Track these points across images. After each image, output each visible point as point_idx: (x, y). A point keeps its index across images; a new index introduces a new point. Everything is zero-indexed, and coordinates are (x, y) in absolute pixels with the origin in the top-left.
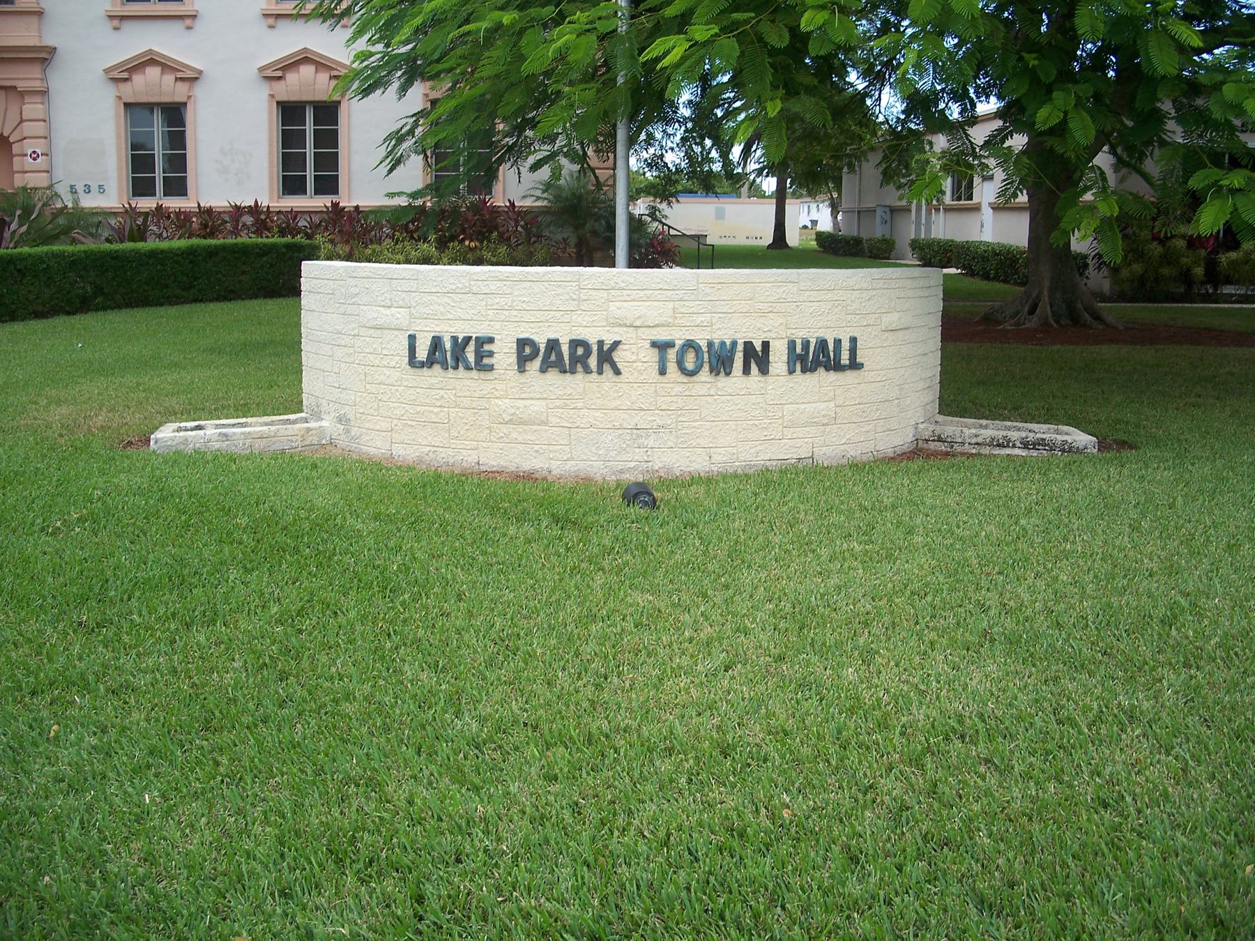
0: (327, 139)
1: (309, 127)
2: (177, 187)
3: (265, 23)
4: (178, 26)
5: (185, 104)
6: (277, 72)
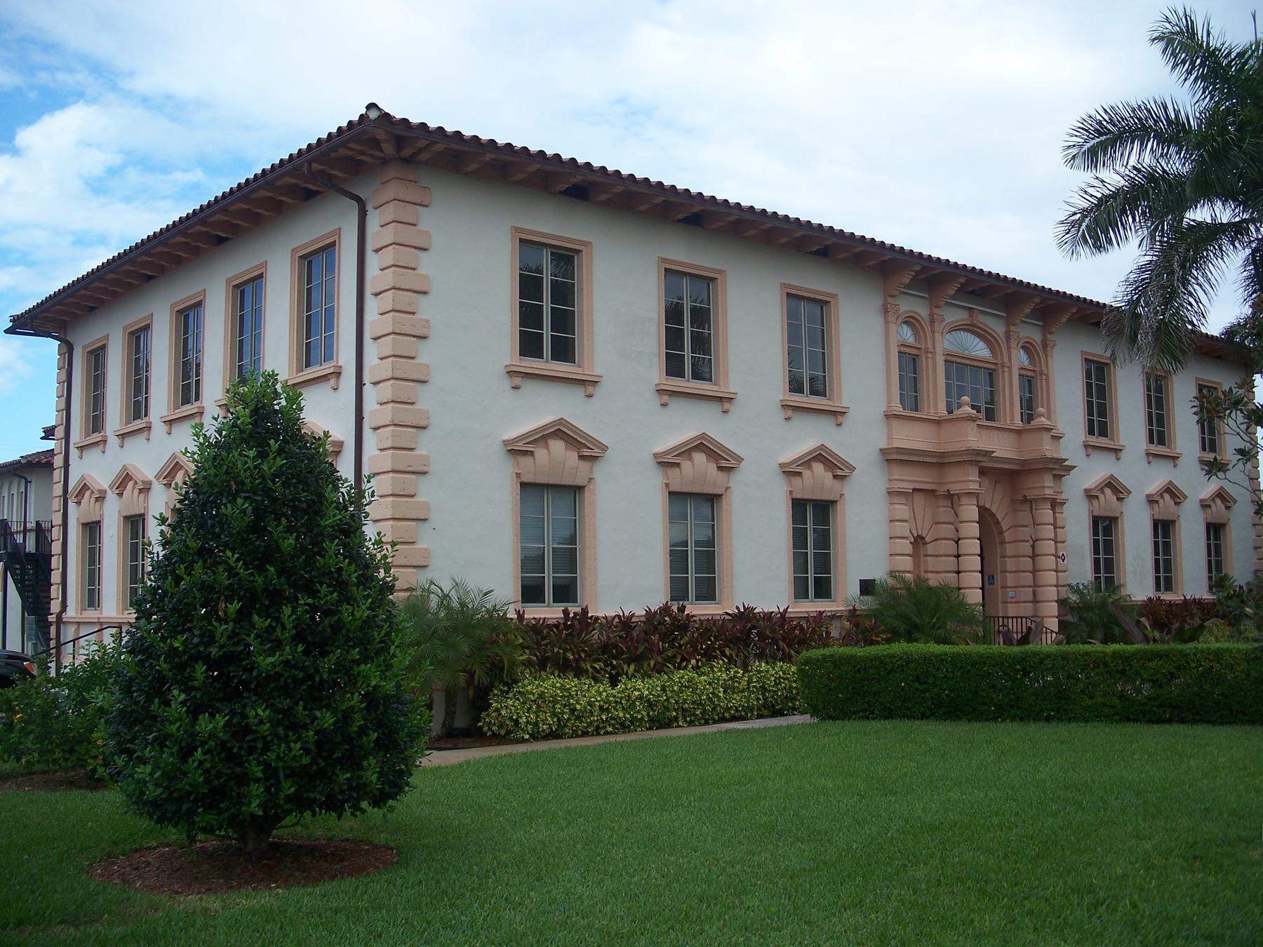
2: (708, 592)
3: (506, 384)
5: (834, 502)
6: (517, 450)
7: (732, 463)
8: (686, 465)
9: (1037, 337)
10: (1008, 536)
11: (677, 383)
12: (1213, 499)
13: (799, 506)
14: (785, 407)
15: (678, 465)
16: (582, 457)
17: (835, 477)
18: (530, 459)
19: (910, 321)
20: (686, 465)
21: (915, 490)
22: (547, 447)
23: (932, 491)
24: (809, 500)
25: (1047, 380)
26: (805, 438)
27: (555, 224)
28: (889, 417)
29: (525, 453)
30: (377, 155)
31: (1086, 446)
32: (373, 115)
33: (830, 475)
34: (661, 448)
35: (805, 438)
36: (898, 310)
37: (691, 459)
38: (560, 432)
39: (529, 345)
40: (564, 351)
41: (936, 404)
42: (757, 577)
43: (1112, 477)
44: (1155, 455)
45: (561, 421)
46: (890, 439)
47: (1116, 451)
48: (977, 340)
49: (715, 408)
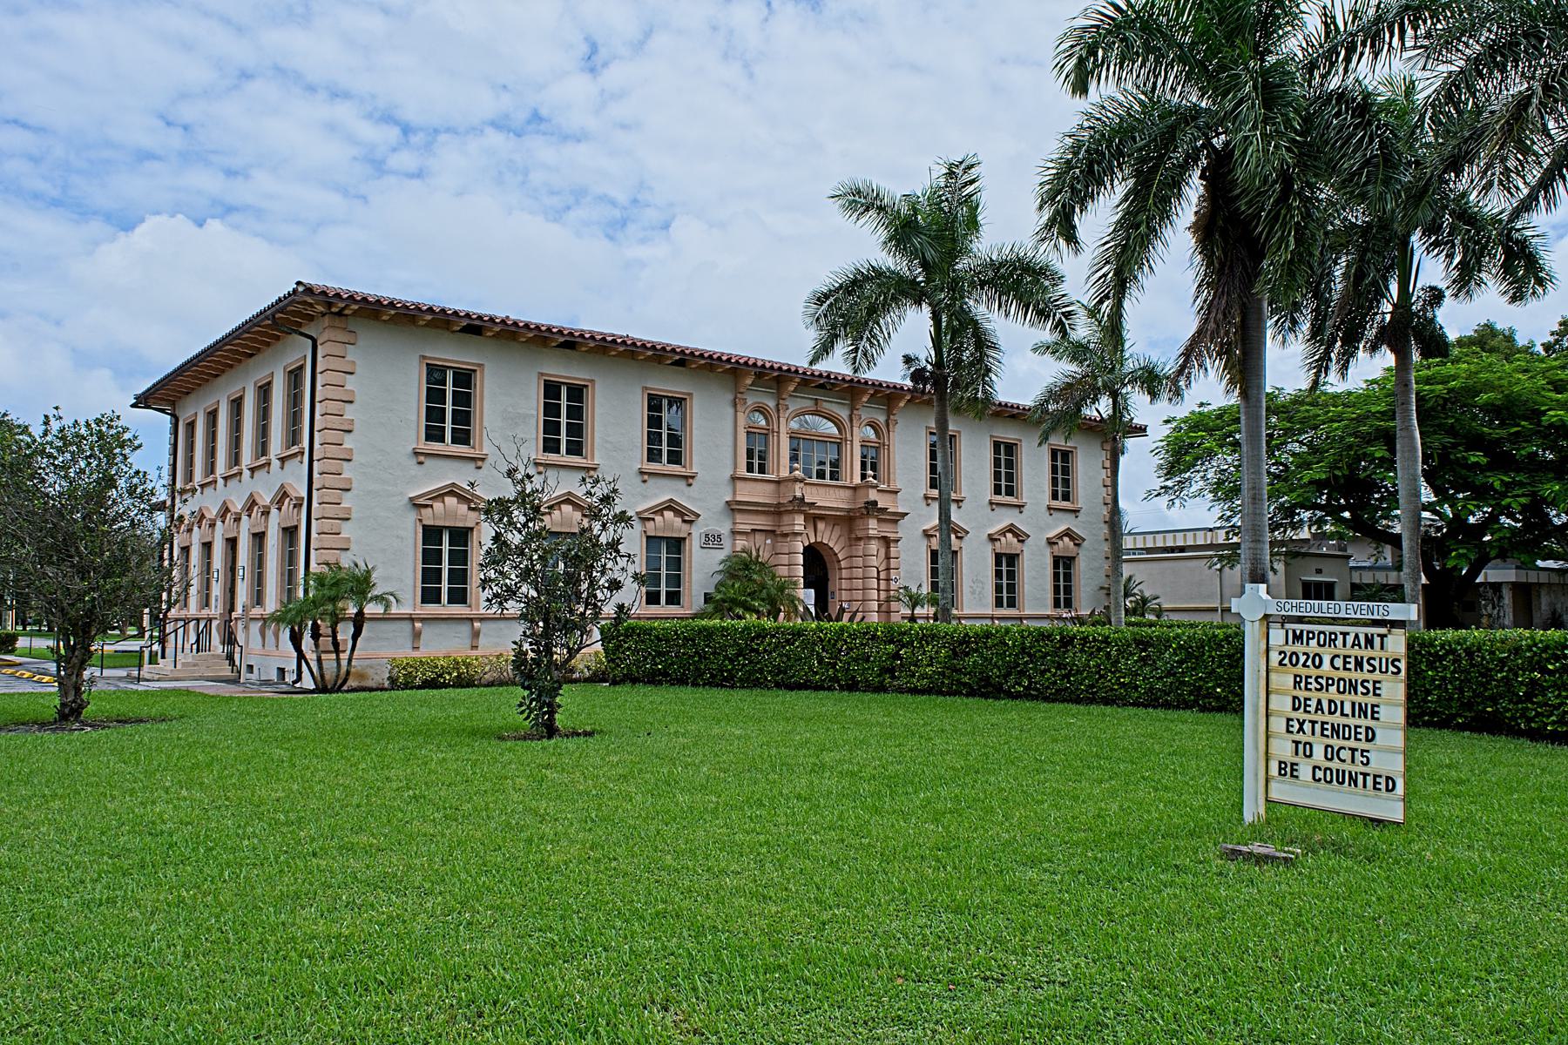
1: (446, 547)
4: (472, 466)
8: (438, 505)
16: (470, 509)
34: (1051, 535)
49: (681, 484)
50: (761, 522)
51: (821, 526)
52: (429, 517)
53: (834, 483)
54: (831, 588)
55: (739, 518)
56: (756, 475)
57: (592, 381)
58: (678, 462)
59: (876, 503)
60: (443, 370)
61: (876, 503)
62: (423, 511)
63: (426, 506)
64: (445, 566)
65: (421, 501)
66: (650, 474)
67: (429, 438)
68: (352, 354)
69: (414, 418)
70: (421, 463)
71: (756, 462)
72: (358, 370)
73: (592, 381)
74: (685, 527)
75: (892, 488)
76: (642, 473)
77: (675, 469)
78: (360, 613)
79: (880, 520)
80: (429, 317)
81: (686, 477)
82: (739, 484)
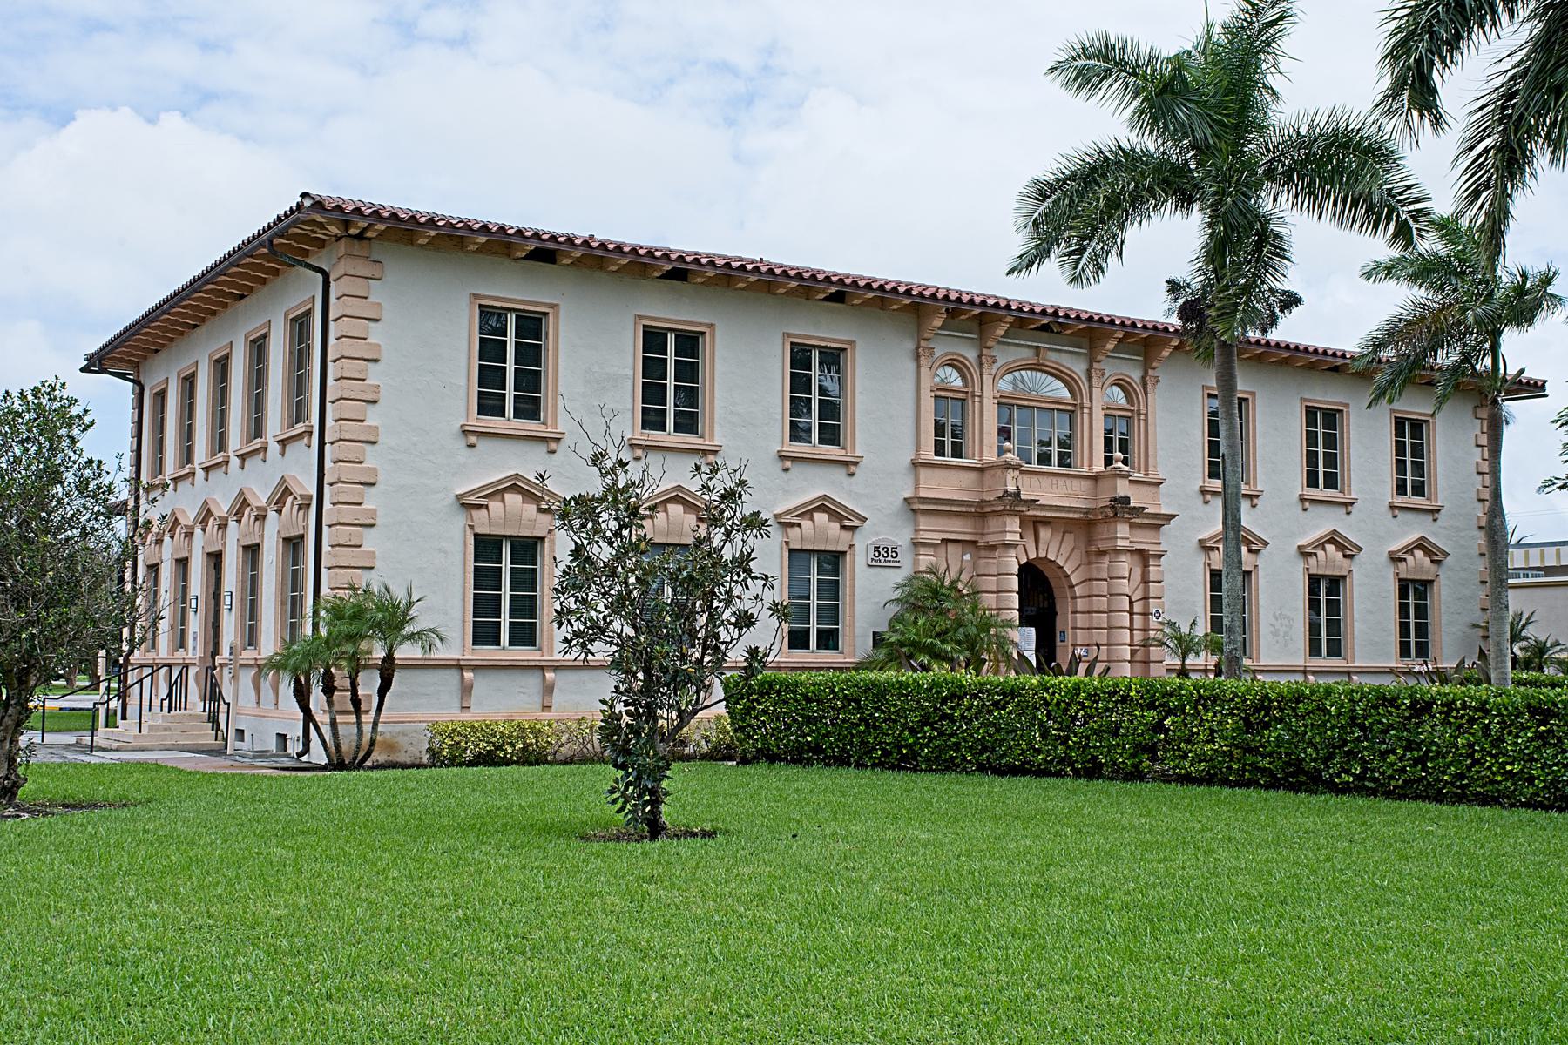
0: (526, 580)
4: (542, 448)
7: (856, 522)
8: (495, 506)
9: (971, 354)
10: (1078, 591)
11: (1313, 492)
12: (1410, 550)
13: (1404, 587)
14: (782, 458)
15: (799, 525)
16: (844, 527)
17: (540, 510)
18: (484, 512)
19: (955, 364)
20: (1410, 559)
21: (945, 541)
22: (812, 519)
23: (975, 542)
24: (1324, 576)
25: (1146, 420)
26: (1411, 530)
27: (517, 290)
28: (916, 465)
29: (792, 525)
30: (316, 238)
31: (1392, 507)
32: (307, 203)
33: (1340, 555)
34: (1395, 547)
35: (1411, 530)
36: (932, 354)
37: (812, 519)
38: (824, 506)
39: (490, 405)
40: (830, 435)
41: (986, 446)
42: (1279, 646)
43: (1423, 538)
44: (1312, 501)
45: (825, 497)
46: (917, 487)
47: (1347, 505)
48: (1050, 379)
49: (839, 473)
50: (958, 528)
51: (1045, 533)
52: (796, 538)
53: (1064, 470)
54: (1059, 627)
55: (924, 522)
56: (948, 459)
57: (852, 343)
58: (834, 441)
59: (1127, 500)
60: (501, 313)
61: (1127, 500)
62: (475, 513)
63: (480, 507)
64: (506, 592)
65: (472, 500)
66: (794, 459)
67: (483, 410)
68: (377, 293)
69: (463, 382)
70: (472, 446)
71: (948, 440)
72: (386, 316)
73: (1347, 405)
74: (846, 535)
75: (1151, 477)
76: (782, 458)
77: (831, 451)
78: (389, 658)
79: (1133, 526)
80: (483, 239)
81: (846, 464)
82: (923, 472)
